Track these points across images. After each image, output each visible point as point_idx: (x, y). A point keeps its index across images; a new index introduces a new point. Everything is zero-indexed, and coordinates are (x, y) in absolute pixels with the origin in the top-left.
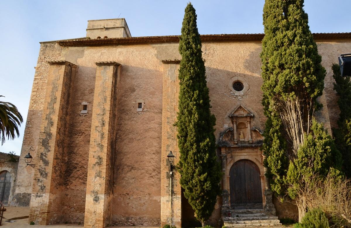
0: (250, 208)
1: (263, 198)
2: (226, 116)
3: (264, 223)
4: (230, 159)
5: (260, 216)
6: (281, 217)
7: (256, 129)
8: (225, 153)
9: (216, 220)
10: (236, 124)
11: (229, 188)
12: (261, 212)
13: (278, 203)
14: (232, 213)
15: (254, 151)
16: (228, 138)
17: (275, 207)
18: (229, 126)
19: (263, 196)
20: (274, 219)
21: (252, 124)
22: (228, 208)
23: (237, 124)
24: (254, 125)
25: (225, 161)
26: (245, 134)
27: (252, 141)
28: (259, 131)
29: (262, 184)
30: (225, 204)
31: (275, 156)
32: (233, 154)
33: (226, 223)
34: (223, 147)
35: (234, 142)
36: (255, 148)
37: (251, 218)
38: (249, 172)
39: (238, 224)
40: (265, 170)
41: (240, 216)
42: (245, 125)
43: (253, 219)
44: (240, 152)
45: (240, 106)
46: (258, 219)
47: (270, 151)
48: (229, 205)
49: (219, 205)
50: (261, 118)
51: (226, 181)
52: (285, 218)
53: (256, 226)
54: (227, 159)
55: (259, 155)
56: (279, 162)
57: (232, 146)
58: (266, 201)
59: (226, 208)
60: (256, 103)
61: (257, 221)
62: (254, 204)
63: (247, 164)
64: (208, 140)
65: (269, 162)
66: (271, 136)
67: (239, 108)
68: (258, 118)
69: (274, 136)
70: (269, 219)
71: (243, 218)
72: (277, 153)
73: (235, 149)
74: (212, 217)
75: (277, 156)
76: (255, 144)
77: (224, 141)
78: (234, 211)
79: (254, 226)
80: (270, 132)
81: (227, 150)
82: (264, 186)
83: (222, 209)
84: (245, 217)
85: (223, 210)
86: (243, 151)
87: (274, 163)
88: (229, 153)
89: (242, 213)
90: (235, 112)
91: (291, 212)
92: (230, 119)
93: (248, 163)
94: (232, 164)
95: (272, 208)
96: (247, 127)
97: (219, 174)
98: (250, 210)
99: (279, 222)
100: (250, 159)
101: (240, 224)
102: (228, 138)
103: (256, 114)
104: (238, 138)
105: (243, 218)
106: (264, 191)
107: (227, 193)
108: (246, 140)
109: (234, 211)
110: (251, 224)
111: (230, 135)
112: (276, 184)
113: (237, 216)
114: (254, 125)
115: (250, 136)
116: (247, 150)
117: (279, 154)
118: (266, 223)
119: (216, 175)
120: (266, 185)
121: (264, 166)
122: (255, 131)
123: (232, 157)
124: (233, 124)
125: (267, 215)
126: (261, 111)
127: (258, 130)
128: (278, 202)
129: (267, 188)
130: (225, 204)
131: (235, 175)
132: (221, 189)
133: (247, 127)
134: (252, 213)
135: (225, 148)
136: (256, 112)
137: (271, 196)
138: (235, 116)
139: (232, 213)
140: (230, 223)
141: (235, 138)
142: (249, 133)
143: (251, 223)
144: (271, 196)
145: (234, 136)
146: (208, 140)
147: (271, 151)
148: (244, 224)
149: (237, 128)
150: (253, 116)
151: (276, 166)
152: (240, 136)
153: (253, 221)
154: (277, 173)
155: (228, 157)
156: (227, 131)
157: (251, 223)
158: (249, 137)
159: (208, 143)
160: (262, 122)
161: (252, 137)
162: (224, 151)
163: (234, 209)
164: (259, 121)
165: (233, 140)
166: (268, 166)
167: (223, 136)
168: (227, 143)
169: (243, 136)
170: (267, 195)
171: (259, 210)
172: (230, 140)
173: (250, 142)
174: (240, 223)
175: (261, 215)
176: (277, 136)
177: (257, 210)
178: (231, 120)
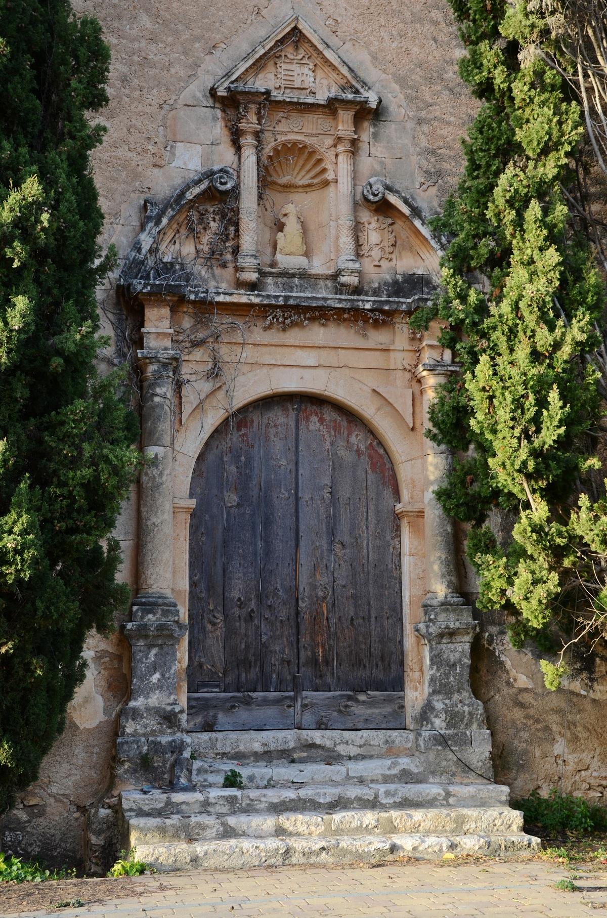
0: (321, 725)
1: (411, 659)
2: (196, 90)
3: (415, 829)
4: (206, 387)
5: (386, 779)
6: (524, 784)
7: (393, 199)
8: (168, 343)
9: (82, 809)
10: (259, 148)
11: (184, 584)
12: (391, 751)
13: (506, 691)
14: (193, 757)
15: (361, 343)
16: (197, 238)
17: (490, 721)
18: (206, 158)
19: (409, 642)
20: (483, 804)
21: (366, 163)
22: (169, 719)
23: (268, 150)
24: (377, 167)
25: (164, 397)
26: (312, 226)
27: (359, 273)
28: (406, 210)
29: (407, 563)
30: (147, 697)
31: (522, 353)
32: (224, 351)
33: (144, 830)
34: (157, 296)
35: (237, 269)
36: (377, 325)
37: (328, 794)
38: (327, 481)
39: (233, 842)
40: (436, 467)
41: (251, 778)
42: (320, 161)
43: (339, 804)
44: (276, 341)
45: (296, 28)
46: (373, 804)
47: (487, 322)
48: (175, 703)
49: (106, 700)
50: (425, 128)
51: (168, 529)
52: (544, 794)
53: (360, 856)
54: (179, 386)
55: (399, 374)
56: (554, 396)
57: (221, 298)
58: (433, 680)
59: (152, 723)
60: (404, 21)
61: (370, 817)
62: (350, 698)
63: (314, 424)
64: (32, 187)
65: (478, 396)
66: (499, 221)
67: (282, 41)
68: (410, 125)
69: (519, 223)
70: (446, 801)
71: (274, 796)
72: (544, 337)
73: (239, 322)
74: (54, 790)
75: (536, 356)
76: (376, 292)
77: (167, 259)
78: (213, 743)
79: (344, 853)
80: (497, 191)
81: (187, 323)
82: (423, 578)
83: (129, 730)
84: (283, 786)
85: (135, 734)
86: (294, 336)
87: (518, 404)
88: (196, 344)
89: (267, 756)
90: (259, 65)
91: (586, 757)
92: (219, 113)
93: (321, 421)
94: (213, 419)
95: (468, 726)
96: (330, 176)
97: (107, 460)
98: (317, 736)
99: (515, 827)
100: (338, 391)
101: (246, 844)
102: (197, 238)
103: (396, 102)
104: (269, 250)
105: (274, 796)
106: (421, 612)
107: (165, 613)
108: (319, 266)
109: (213, 743)
110: (323, 844)
111: (212, 224)
112: (522, 553)
113: (232, 781)
114: (377, 167)
115: (346, 241)
116: (319, 334)
117: (557, 346)
118: (428, 833)
119: (87, 472)
120: (436, 567)
121: (434, 438)
122: (383, 208)
123: (215, 373)
124: (238, 148)
125: (433, 773)
126: (430, 80)
127: (406, 202)
128: (508, 684)
129: (440, 590)
130: (148, 690)
131: (232, 498)
132: (122, 576)
133: (330, 176)
134: (331, 757)
135: (174, 310)
136: (402, 81)
137: (467, 647)
138: (258, 94)
139: (193, 757)
140: (176, 836)
141: (248, 242)
142: (346, 222)
143: (322, 835)
144: (462, 647)
145: (237, 231)
146: (32, 187)
147: (494, 328)
148: (273, 843)
149: (265, 182)
150: (374, 105)
151: (525, 432)
152: (280, 234)
153: (337, 817)
154: (529, 477)
155: (186, 370)
156: (196, 191)
157: (322, 835)
158: (338, 250)
159: (31, 209)
160: (434, 152)
161: (358, 245)
162: (165, 327)
163: (208, 727)
164: (412, 150)
165: (229, 257)
166: (472, 422)
167: (165, 221)
168: (188, 277)
169: (298, 240)
170: (441, 636)
171: (376, 737)
172: (214, 257)
173: (343, 279)
174: (244, 834)
175: (395, 771)
176: (542, 223)
177: (365, 733)
178: (227, 120)
